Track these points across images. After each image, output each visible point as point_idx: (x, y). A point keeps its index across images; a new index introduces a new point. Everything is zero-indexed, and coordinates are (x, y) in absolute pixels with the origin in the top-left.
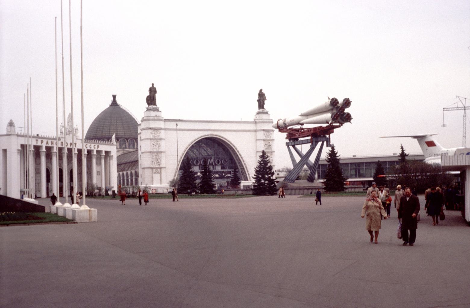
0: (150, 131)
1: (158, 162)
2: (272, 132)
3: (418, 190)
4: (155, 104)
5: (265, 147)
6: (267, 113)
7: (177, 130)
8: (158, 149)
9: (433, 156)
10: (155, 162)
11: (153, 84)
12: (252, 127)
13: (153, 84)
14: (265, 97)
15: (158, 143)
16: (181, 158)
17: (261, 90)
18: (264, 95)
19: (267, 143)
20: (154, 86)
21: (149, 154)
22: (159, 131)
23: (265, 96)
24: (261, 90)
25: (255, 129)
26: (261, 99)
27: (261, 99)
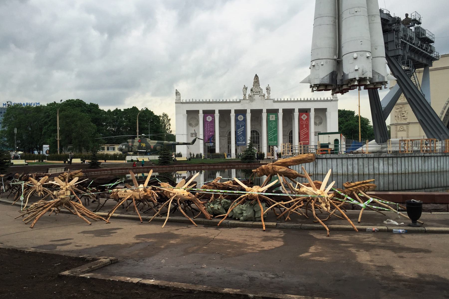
1: (404, 116)
10: (399, 116)
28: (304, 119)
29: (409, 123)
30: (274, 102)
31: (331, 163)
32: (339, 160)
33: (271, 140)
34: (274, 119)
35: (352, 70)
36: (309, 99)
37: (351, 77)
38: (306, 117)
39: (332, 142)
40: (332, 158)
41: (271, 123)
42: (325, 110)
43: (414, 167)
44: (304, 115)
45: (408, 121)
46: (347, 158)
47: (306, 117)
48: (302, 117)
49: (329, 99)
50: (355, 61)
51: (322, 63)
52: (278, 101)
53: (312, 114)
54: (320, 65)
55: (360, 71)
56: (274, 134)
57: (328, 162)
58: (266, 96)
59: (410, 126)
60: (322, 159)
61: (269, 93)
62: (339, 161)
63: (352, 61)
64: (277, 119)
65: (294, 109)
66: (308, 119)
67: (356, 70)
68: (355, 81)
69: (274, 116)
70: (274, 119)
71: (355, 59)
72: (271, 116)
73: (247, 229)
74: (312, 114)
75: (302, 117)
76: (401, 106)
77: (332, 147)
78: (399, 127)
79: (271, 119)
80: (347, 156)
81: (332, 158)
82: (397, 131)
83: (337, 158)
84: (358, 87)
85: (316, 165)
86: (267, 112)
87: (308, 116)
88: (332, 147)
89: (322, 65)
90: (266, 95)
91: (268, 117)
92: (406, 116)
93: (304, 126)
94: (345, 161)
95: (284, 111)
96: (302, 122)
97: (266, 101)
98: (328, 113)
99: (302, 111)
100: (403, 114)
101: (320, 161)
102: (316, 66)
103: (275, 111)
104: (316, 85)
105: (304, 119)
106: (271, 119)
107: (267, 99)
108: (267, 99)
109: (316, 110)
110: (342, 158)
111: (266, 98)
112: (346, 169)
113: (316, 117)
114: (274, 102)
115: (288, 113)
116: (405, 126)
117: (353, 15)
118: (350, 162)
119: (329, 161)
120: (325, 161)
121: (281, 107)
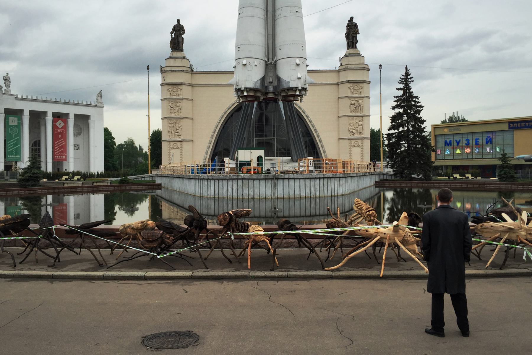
0: (349, 85)
1: (178, 133)
2: (365, 85)
3: (444, 191)
4: (182, 50)
5: (350, 109)
6: (185, 58)
7: (193, 86)
8: (177, 114)
9: (74, 141)
10: (173, 132)
11: (178, 21)
12: (332, 78)
13: (178, 21)
14: (358, 30)
15: (178, 104)
16: (312, 125)
17: (352, 18)
18: (356, 26)
19: (353, 102)
20: (181, 23)
21: (347, 118)
23: (357, 28)
24: (352, 18)
25: (336, 81)
26: (352, 31)
27: (352, 31)
28: (60, 127)
29: (183, 141)
30: (17, 99)
31: (293, 184)
32: (301, 180)
33: (12, 153)
34: (16, 123)
35: (295, 77)
36: (67, 101)
37: (293, 85)
38: (63, 124)
39: (255, 160)
40: (294, 179)
41: (11, 130)
42: (86, 118)
43: (216, 186)
44: (60, 121)
45: (182, 138)
46: (310, 178)
47: (63, 124)
48: (57, 124)
49: (93, 104)
50: (297, 67)
51: (256, 64)
52: (22, 99)
53: (71, 121)
54: (254, 66)
55: (302, 80)
56: (15, 145)
57: (290, 183)
58: (3, 89)
59: (184, 143)
60: (283, 179)
61: (8, 86)
62: (302, 181)
63: (294, 67)
64: (21, 123)
65: (46, 112)
66: (65, 128)
67: (299, 78)
68: (295, 91)
69: (16, 119)
70: (16, 123)
71: (298, 65)
72: (11, 119)
73: (149, 282)
74: (71, 121)
75: (57, 124)
76: (174, 121)
77: (254, 165)
78: (172, 143)
79: (11, 124)
80: (311, 176)
81: (294, 179)
82: (170, 148)
83: (300, 179)
84: (299, 98)
85: (275, 187)
86: (5, 113)
87: (66, 122)
88: (254, 165)
89: (256, 65)
90: (4, 88)
91: (54, 122)
92: (180, 132)
93: (59, 136)
94: (308, 181)
95: (32, 113)
96: (57, 131)
97: (5, 96)
98: (91, 122)
99: (57, 116)
100: (177, 129)
101: (280, 182)
102: (248, 66)
103: (18, 113)
104: (246, 88)
105: (60, 127)
106: (11, 124)
107: (5, 94)
108: (5, 94)
109: (76, 116)
110: (305, 178)
111: (4, 92)
112: (309, 191)
113: (75, 125)
114: (17, 99)
115: (37, 117)
116: (178, 143)
117: (292, 14)
118: (313, 182)
119: (292, 182)
120: (286, 182)
121: (27, 107)
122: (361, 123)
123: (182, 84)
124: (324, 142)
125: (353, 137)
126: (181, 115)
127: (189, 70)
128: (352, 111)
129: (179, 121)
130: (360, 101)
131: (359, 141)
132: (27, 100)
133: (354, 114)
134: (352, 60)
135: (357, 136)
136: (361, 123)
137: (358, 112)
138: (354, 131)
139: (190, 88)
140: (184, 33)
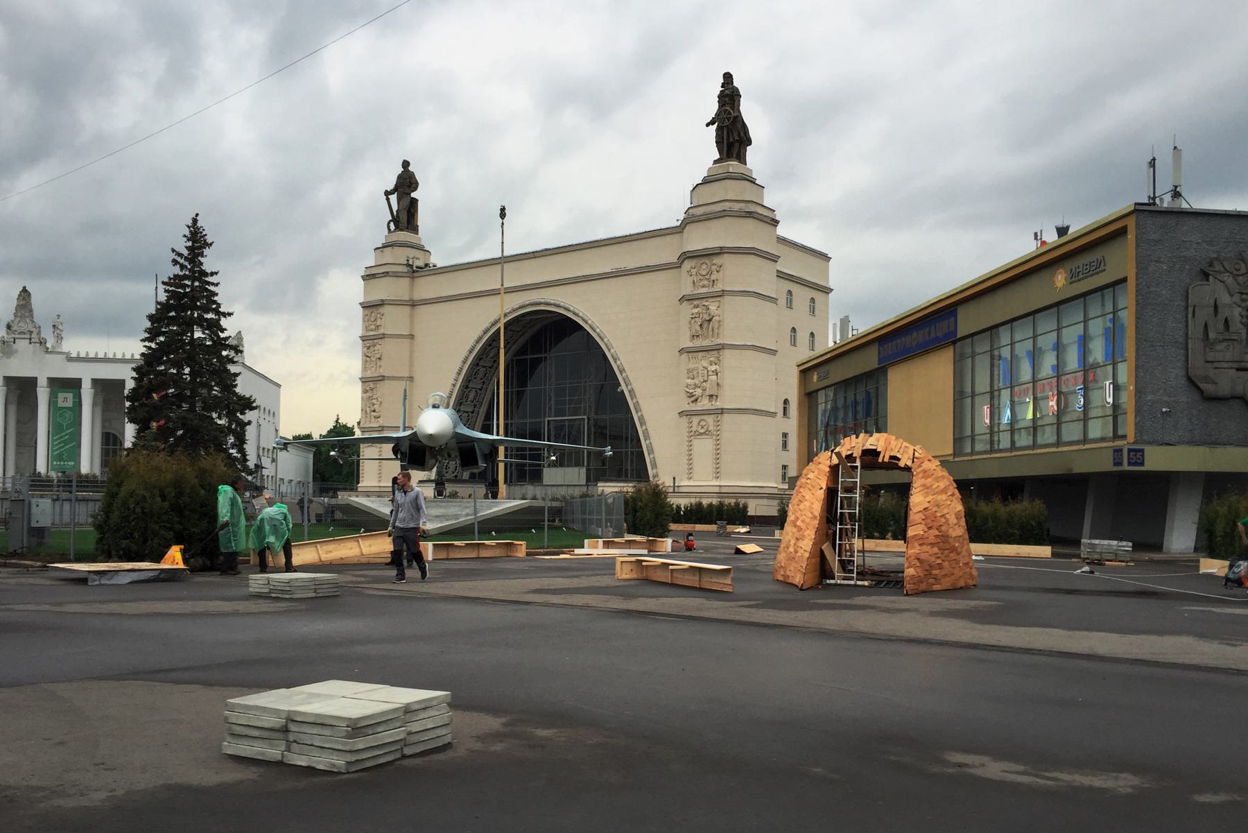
7: (413, 304)
11: (406, 164)
12: (667, 252)
13: (406, 164)
22: (717, 260)
34: (70, 404)
69: (70, 396)
70: (70, 404)
72: (61, 396)
79: (60, 404)
95: (95, 382)
106: (60, 404)
109: (95, 382)
122: (713, 368)
123: (721, 251)
124: (651, 425)
125: (694, 407)
126: (382, 372)
127: (405, 269)
128: (694, 337)
129: (380, 384)
130: (713, 308)
131: (710, 420)
132: (87, 360)
133: (699, 343)
134: (732, 190)
135: (704, 404)
136: (713, 368)
137: (706, 337)
138: (698, 392)
139: (407, 309)
140: (415, 189)
